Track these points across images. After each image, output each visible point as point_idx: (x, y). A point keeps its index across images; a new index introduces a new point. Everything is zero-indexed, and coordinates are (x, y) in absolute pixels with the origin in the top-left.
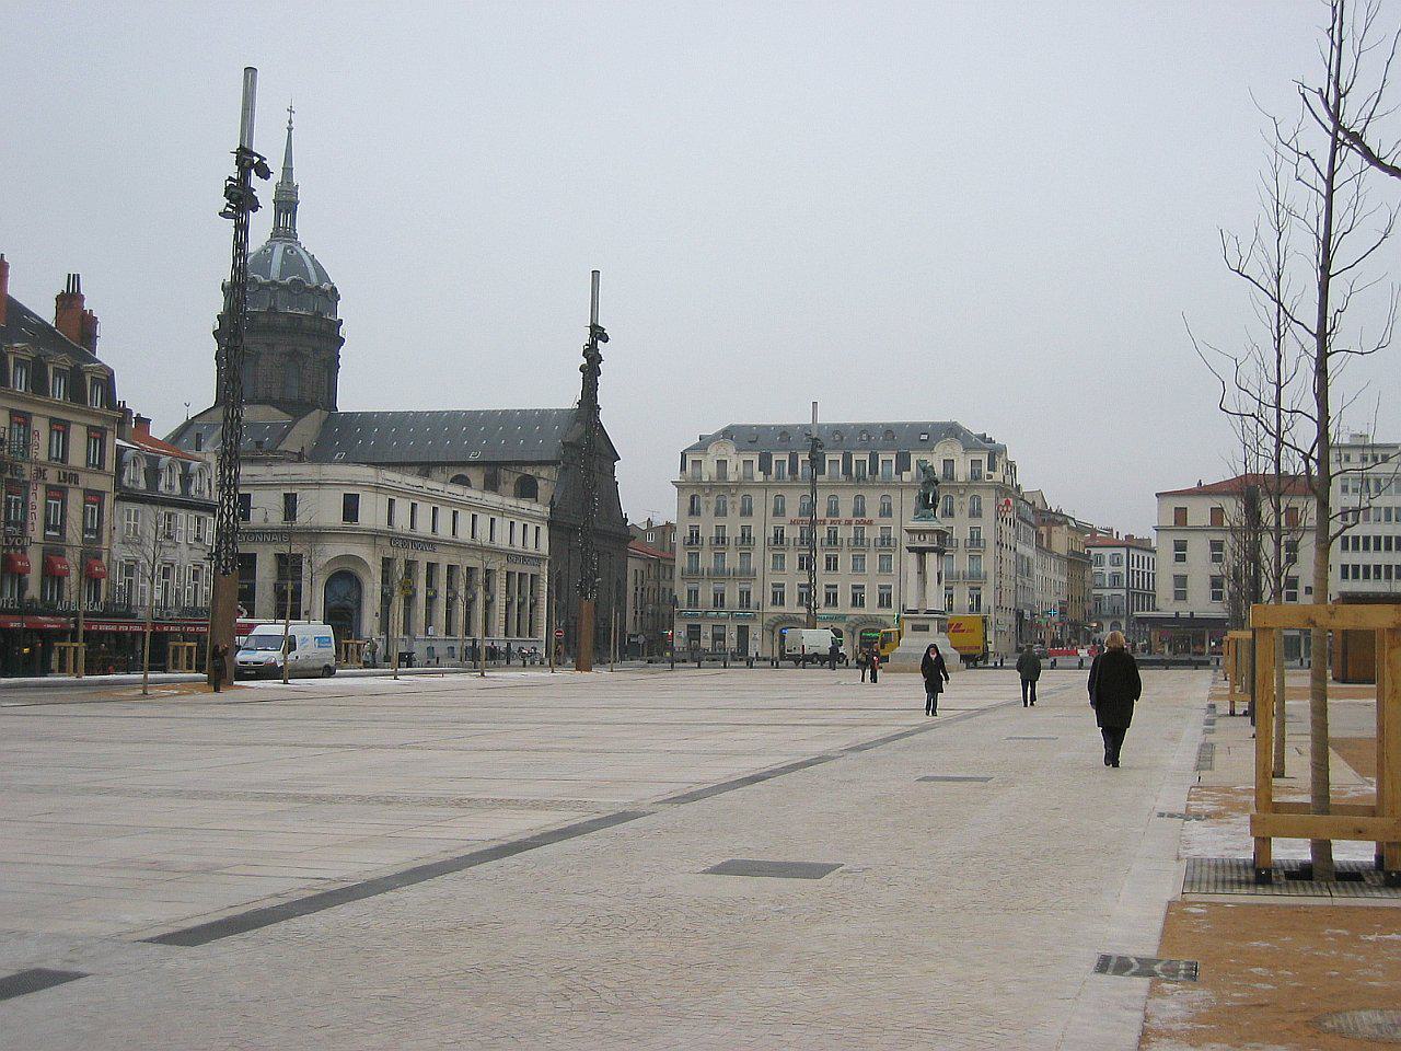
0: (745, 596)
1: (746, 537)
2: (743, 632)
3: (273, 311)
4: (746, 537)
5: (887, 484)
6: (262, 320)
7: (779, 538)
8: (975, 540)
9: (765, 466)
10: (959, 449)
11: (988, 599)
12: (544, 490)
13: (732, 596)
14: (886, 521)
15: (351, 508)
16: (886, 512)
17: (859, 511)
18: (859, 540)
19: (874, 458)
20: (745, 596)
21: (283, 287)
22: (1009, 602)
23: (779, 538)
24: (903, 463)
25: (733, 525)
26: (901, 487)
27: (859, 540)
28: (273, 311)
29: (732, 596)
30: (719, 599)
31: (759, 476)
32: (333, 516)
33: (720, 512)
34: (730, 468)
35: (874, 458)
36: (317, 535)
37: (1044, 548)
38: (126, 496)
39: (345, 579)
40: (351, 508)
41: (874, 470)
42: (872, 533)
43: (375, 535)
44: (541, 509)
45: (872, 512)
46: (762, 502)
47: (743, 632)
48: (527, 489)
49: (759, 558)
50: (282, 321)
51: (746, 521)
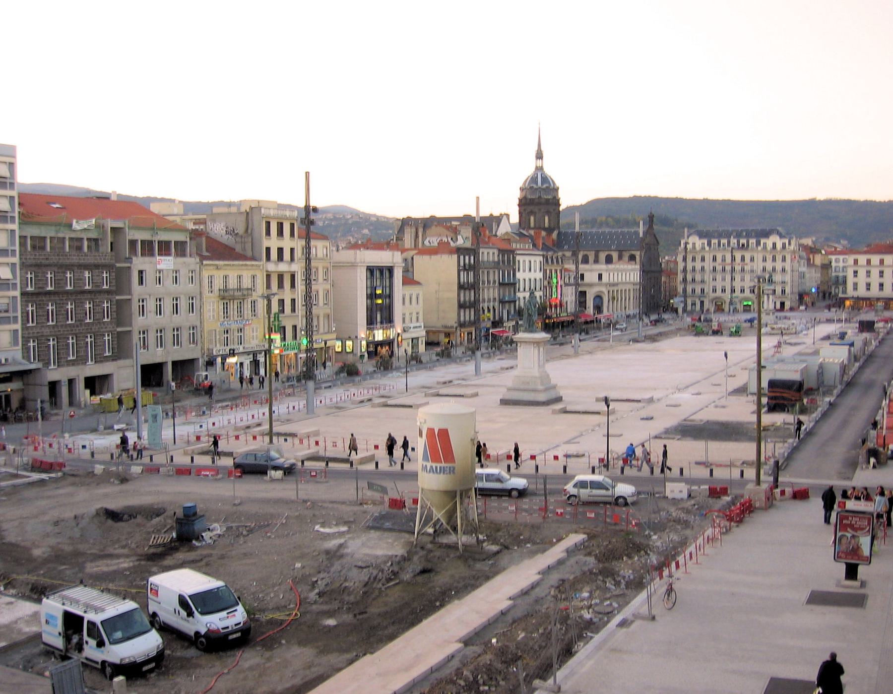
0: (703, 291)
1: (703, 268)
2: (702, 303)
3: (540, 197)
4: (703, 268)
5: (752, 249)
6: (537, 201)
7: (714, 269)
8: (784, 270)
9: (709, 244)
10: (778, 238)
11: (788, 290)
12: (638, 258)
13: (698, 291)
14: (752, 264)
15: (600, 277)
16: (752, 259)
17: (743, 258)
18: (743, 270)
19: (748, 242)
20: (703, 291)
21: (544, 189)
22: (796, 290)
23: (714, 269)
24: (758, 243)
25: (698, 265)
26: (758, 252)
27: (743, 270)
28: (540, 197)
29: (698, 291)
30: (693, 291)
31: (707, 248)
32: (596, 279)
33: (774, 259)
34: (697, 246)
35: (748, 242)
36: (591, 285)
37: (810, 264)
38: (566, 285)
39: (598, 298)
40: (600, 277)
41: (748, 245)
42: (747, 268)
43: (606, 285)
44: (638, 267)
45: (747, 259)
46: (708, 257)
47: (702, 303)
48: (632, 258)
49: (708, 277)
50: (543, 201)
51: (703, 264)
